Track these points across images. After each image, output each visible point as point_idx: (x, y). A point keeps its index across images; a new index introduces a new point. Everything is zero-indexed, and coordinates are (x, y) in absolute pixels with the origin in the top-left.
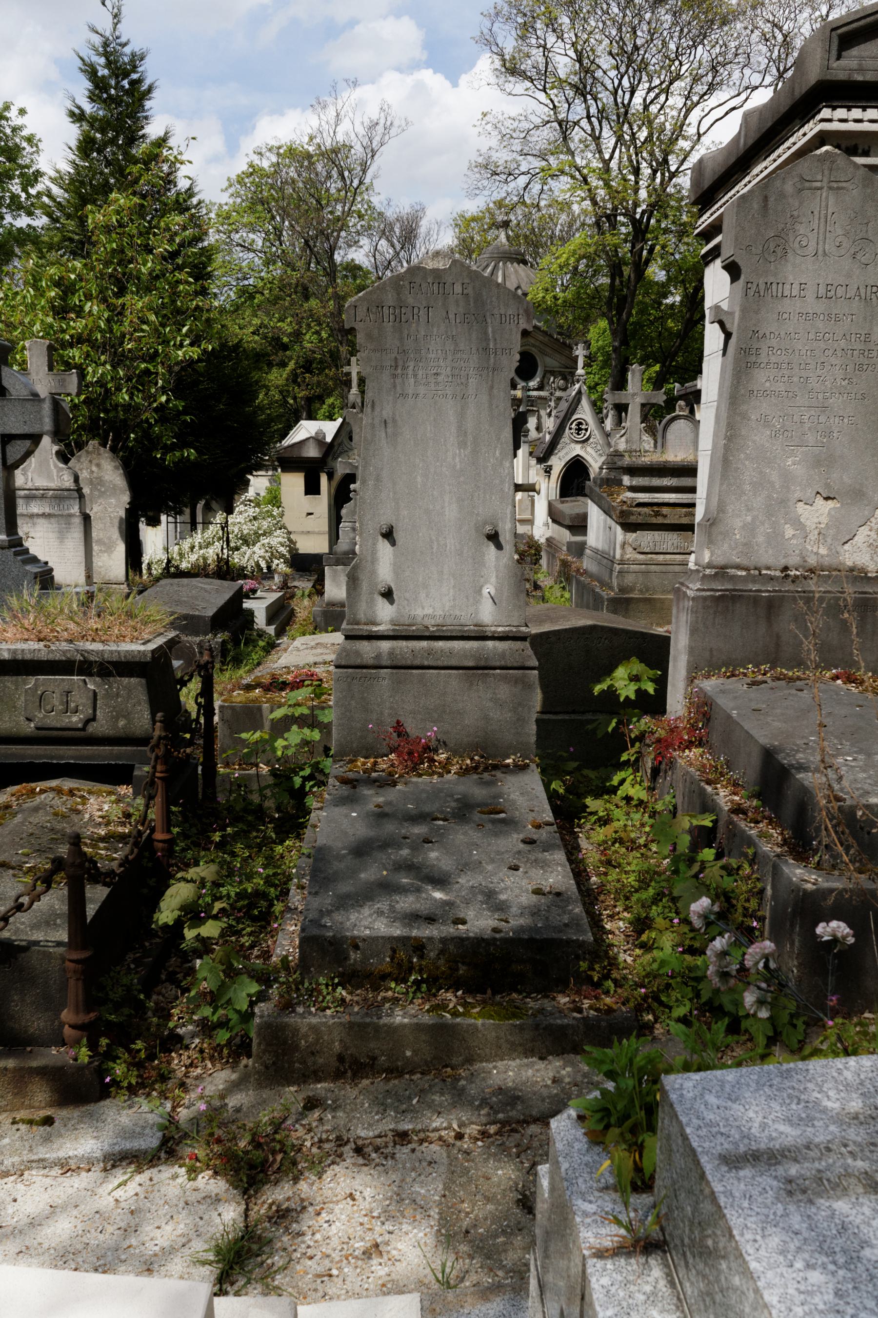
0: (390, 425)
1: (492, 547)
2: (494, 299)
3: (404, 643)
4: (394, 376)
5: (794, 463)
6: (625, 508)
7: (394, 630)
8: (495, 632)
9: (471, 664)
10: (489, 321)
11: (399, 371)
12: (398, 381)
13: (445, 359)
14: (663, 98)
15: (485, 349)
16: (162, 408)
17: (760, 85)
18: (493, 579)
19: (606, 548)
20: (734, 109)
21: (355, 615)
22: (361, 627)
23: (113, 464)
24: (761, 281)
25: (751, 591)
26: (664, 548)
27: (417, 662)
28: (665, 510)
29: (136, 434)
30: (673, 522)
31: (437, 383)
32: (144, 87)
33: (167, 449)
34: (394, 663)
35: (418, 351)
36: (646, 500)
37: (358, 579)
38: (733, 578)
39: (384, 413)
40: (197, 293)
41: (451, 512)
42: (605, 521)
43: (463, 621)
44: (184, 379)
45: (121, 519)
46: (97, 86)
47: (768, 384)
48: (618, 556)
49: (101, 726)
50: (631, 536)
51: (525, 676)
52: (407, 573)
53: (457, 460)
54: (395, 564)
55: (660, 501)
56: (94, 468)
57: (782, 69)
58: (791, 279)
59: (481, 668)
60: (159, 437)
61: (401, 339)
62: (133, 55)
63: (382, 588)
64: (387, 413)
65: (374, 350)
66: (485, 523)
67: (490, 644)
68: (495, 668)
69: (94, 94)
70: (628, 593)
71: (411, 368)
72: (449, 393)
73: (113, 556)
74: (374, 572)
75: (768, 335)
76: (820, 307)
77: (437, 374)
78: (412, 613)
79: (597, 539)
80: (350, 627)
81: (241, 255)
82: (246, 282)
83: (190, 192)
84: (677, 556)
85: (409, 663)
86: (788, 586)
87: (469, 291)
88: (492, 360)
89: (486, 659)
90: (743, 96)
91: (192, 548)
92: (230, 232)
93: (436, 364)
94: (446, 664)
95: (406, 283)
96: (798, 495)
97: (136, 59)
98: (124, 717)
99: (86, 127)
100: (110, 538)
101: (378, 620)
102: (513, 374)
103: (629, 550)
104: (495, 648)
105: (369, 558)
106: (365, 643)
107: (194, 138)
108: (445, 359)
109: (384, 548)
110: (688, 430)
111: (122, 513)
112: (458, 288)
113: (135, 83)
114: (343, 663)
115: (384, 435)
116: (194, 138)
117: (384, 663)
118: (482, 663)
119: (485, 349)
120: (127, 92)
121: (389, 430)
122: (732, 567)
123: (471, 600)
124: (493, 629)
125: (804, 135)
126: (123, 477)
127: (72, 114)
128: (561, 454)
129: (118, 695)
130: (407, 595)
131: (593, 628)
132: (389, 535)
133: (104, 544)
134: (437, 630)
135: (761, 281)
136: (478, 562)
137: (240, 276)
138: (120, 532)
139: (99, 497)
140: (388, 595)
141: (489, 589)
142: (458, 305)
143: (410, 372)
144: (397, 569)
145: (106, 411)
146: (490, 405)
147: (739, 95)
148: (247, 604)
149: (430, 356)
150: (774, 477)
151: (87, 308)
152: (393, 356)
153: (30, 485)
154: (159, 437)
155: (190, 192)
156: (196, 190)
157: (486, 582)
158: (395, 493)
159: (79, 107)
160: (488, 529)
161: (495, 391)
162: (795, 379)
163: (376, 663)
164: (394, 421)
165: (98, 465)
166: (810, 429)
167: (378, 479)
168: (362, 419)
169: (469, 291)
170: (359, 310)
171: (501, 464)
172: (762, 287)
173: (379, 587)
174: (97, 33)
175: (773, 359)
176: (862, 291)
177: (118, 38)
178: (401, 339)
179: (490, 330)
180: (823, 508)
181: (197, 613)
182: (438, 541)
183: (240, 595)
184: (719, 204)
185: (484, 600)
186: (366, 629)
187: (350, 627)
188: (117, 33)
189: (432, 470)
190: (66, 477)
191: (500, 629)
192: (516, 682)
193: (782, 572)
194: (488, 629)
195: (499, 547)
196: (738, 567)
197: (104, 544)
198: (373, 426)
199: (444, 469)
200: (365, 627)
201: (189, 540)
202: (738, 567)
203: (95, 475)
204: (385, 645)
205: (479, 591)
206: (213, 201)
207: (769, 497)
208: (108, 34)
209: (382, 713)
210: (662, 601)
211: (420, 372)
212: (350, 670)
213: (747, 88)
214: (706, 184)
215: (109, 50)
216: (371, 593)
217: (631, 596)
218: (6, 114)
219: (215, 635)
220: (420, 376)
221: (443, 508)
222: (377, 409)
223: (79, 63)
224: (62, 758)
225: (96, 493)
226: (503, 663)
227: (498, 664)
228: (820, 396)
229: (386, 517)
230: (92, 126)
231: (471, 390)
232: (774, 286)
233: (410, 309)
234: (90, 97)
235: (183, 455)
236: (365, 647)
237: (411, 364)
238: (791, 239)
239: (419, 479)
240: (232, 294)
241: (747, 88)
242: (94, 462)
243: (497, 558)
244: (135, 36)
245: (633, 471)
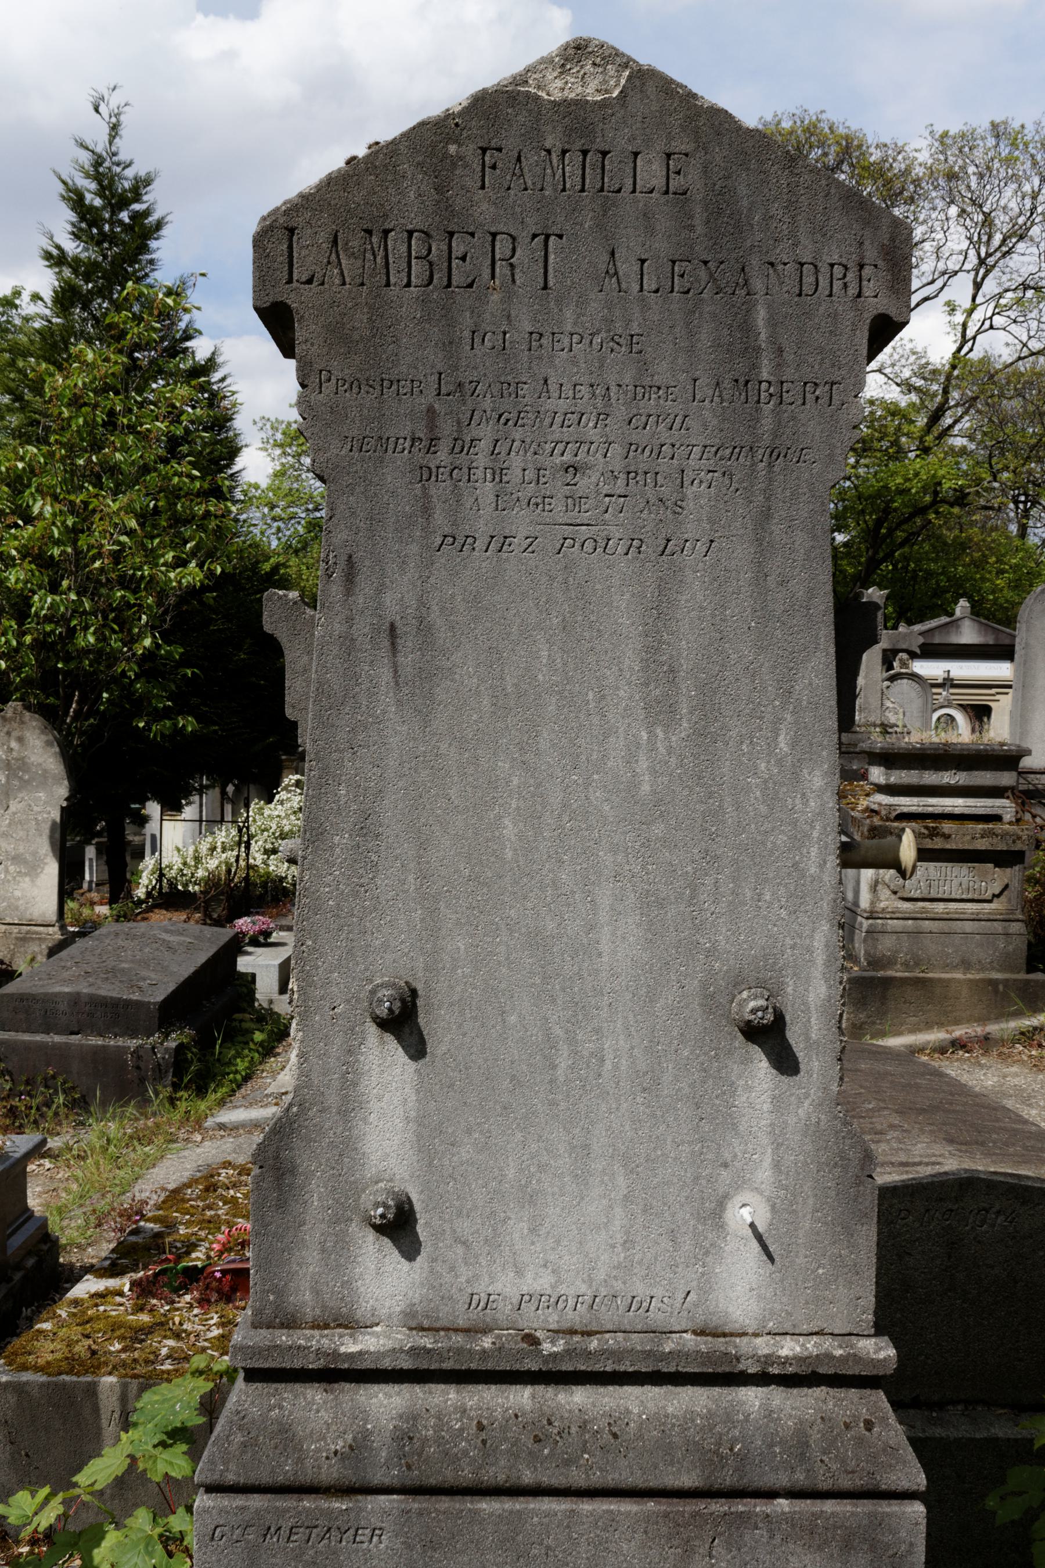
0: (408, 642)
1: (761, 1065)
2: (776, 209)
3: (450, 1395)
4: (426, 474)
6: (876, 821)
7: (415, 1352)
8: (769, 1359)
9: (688, 1480)
10: (758, 284)
11: (443, 455)
12: (439, 490)
13: (603, 416)
16: (150, 655)
17: (960, 270)
18: (764, 1174)
20: (926, 299)
21: (280, 1293)
22: (300, 1338)
23: (44, 737)
26: (944, 891)
27: (497, 1474)
28: (947, 827)
29: (111, 694)
30: (961, 847)
31: (575, 500)
32: (152, 219)
33: (159, 715)
34: (414, 1477)
35: (510, 387)
36: (913, 809)
37: (293, 1171)
39: (389, 599)
40: (205, 494)
41: (619, 942)
43: (656, 1317)
44: (184, 615)
45: (54, 823)
46: (82, 218)
51: (877, 1522)
52: (466, 1152)
53: (643, 764)
54: (421, 1120)
55: (938, 810)
56: (14, 744)
57: (983, 255)
59: (724, 1489)
60: (146, 697)
61: (450, 345)
62: (137, 179)
63: (375, 1202)
64: (397, 600)
65: (355, 384)
66: (738, 983)
67: (752, 1397)
68: (771, 1494)
69: (81, 229)
70: (883, 967)
71: (484, 445)
72: (616, 533)
73: (39, 882)
74: (347, 1148)
77: (573, 468)
78: (482, 1288)
80: (263, 1337)
81: (312, 482)
82: (318, 514)
83: (211, 364)
84: (969, 905)
85: (466, 1475)
87: (692, 179)
88: (767, 423)
89: (742, 1458)
90: (939, 283)
91: (213, 849)
92: (300, 455)
93: (567, 434)
94: (597, 1479)
95: (470, 150)
97: (140, 185)
99: (67, 273)
100: (34, 854)
101: (363, 1310)
103: (884, 893)
104: (769, 1413)
105: (333, 1100)
106: (315, 1394)
107: (203, 275)
108: (603, 416)
109: (384, 1062)
110: (913, 694)
111: (56, 815)
112: (651, 171)
113: (138, 217)
114: (231, 1478)
115: (386, 675)
116: (203, 275)
117: (378, 1477)
118: (728, 1479)
120: (127, 228)
121: (407, 660)
123: (687, 1245)
124: (763, 1346)
126: (60, 759)
127: (48, 256)
130: (465, 1227)
131: (966, 1185)
132: (403, 1022)
133: (25, 862)
134: (568, 1353)
136: (715, 1116)
137: (311, 506)
138: (52, 844)
139: (20, 789)
140: (399, 1226)
141: (745, 1212)
142: (650, 231)
143: (482, 460)
144: (429, 1135)
145: (67, 660)
146: (761, 576)
147: (933, 282)
148: (244, 964)
149: (551, 404)
151: (36, 510)
152: (422, 402)
154: (146, 697)
155: (211, 364)
156: (220, 360)
157: (740, 1183)
158: (424, 877)
159: (58, 247)
160: (751, 1004)
161: (777, 528)
163: (350, 1477)
164: (424, 628)
165: (20, 740)
167: (366, 828)
168: (312, 623)
169: (692, 179)
170: (303, 239)
171: (796, 777)
173: (367, 1199)
174: (87, 148)
177: (114, 154)
178: (450, 345)
179: (761, 314)
181: (136, 996)
182: (572, 1041)
183: (235, 947)
185: (730, 1246)
186: (315, 1343)
187: (263, 1337)
188: (114, 149)
189: (556, 798)
191: (788, 1348)
192: (847, 1546)
195: (785, 1062)
197: (25, 862)
198: (348, 644)
199: (597, 795)
201: (210, 839)
203: (15, 754)
204: (385, 1403)
205: (715, 1215)
206: (280, 419)
208: (99, 149)
210: (946, 983)
211: (516, 461)
212: (256, 1501)
213: (944, 273)
215: (102, 170)
216: (335, 1221)
217: (890, 973)
218: (17, 302)
219: (167, 1036)
220: (514, 474)
221: (591, 928)
222: (365, 586)
223: (60, 188)
225: (16, 782)
226: (800, 1478)
227: (783, 1480)
229: (391, 958)
230: (75, 271)
231: (693, 526)
233: (481, 240)
234: (73, 233)
235: (175, 725)
236: (312, 1407)
237: (486, 433)
239: (509, 829)
240: (299, 528)
241: (944, 273)
242: (15, 734)
243: (778, 1103)
244: (137, 155)
245: (890, 759)
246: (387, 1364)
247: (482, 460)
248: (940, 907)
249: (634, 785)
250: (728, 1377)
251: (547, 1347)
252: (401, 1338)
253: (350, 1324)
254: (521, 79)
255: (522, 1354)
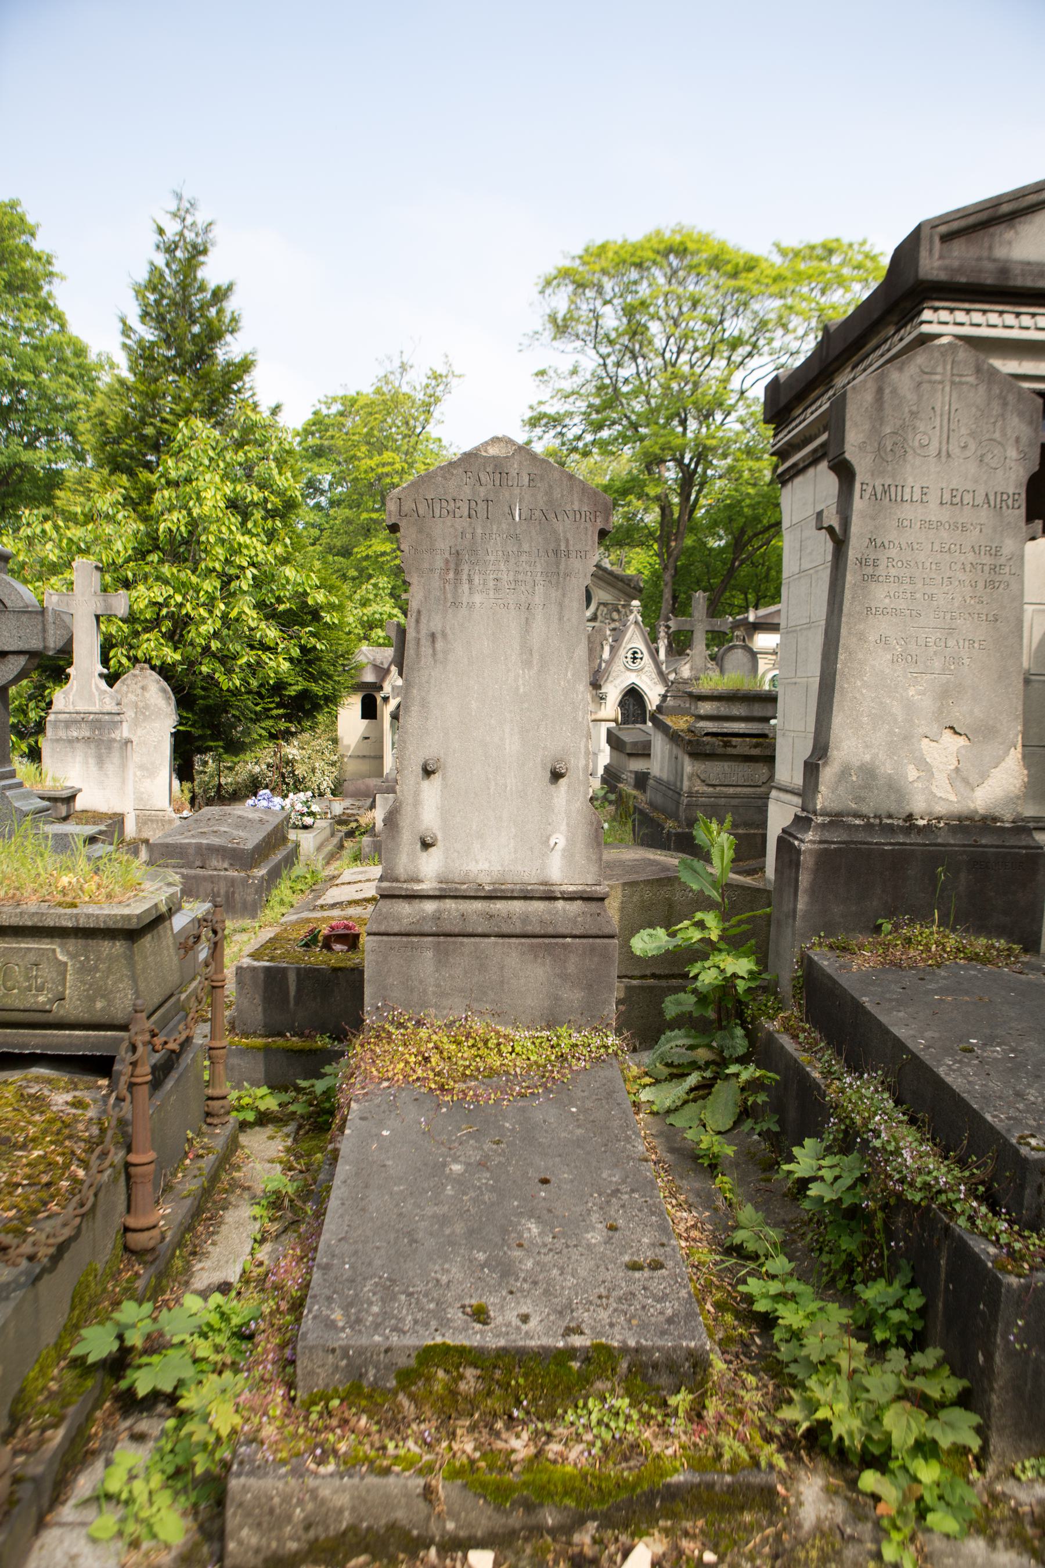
5: (919, 693)
7: (441, 889)
14: (707, 359)
15: (556, 552)
18: (563, 827)
19: (672, 778)
24: (878, 483)
25: (871, 843)
26: (734, 780)
36: (714, 730)
38: (851, 827)
39: (432, 624)
41: (512, 745)
42: (671, 751)
43: (526, 879)
47: (887, 601)
48: (685, 788)
49: (72, 1008)
50: (701, 767)
53: (521, 682)
58: (910, 481)
67: (560, 904)
68: (565, 937)
71: (466, 572)
74: (417, 816)
75: (886, 544)
76: (944, 515)
79: (661, 770)
86: (914, 838)
96: (923, 730)
98: (103, 996)
101: (421, 876)
102: (588, 581)
110: (745, 660)
118: (550, 930)
119: (556, 552)
122: (848, 815)
124: (564, 888)
125: (901, 340)
128: (617, 682)
129: (96, 969)
133: (148, 770)
135: (878, 483)
139: (144, 720)
143: (465, 577)
144: (445, 814)
146: (560, 619)
150: (897, 709)
153: (71, 709)
162: (918, 596)
164: (444, 635)
166: (935, 653)
172: (879, 489)
175: (893, 572)
176: (992, 498)
180: (952, 743)
184: (794, 424)
190: (107, 700)
191: (571, 888)
193: (905, 821)
194: (554, 888)
196: (856, 815)
197: (148, 770)
200: (405, 886)
202: (856, 815)
204: (430, 906)
207: (891, 732)
209: (425, 991)
214: (783, 401)
220: (476, 581)
224: (26, 1047)
228: (948, 616)
232: (893, 489)
236: (405, 909)
237: (465, 568)
238: (910, 436)
239: (474, 705)
246: (431, 893)
247: (465, 577)
248: (731, 790)
249: (517, 688)
250: (551, 898)
251: (487, 888)
252: (435, 885)
253: (419, 881)
254: (477, 449)
255: (477, 890)
